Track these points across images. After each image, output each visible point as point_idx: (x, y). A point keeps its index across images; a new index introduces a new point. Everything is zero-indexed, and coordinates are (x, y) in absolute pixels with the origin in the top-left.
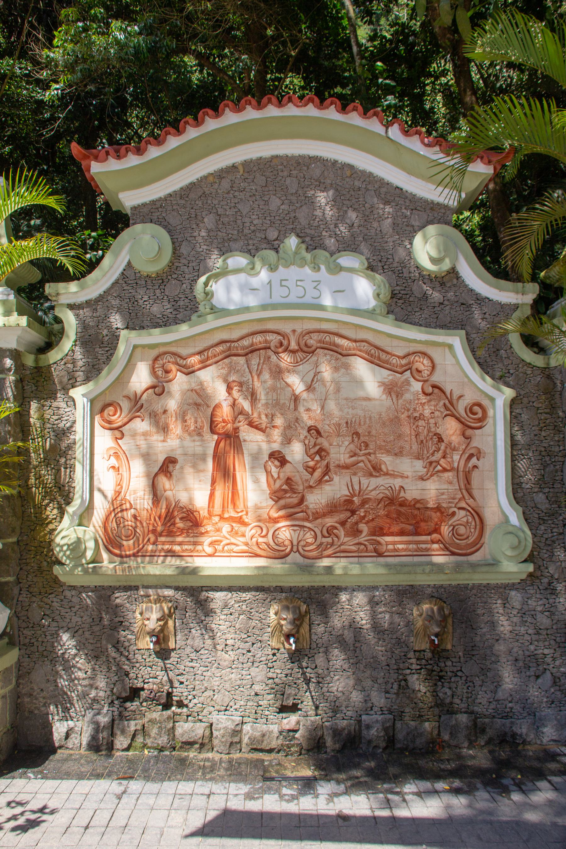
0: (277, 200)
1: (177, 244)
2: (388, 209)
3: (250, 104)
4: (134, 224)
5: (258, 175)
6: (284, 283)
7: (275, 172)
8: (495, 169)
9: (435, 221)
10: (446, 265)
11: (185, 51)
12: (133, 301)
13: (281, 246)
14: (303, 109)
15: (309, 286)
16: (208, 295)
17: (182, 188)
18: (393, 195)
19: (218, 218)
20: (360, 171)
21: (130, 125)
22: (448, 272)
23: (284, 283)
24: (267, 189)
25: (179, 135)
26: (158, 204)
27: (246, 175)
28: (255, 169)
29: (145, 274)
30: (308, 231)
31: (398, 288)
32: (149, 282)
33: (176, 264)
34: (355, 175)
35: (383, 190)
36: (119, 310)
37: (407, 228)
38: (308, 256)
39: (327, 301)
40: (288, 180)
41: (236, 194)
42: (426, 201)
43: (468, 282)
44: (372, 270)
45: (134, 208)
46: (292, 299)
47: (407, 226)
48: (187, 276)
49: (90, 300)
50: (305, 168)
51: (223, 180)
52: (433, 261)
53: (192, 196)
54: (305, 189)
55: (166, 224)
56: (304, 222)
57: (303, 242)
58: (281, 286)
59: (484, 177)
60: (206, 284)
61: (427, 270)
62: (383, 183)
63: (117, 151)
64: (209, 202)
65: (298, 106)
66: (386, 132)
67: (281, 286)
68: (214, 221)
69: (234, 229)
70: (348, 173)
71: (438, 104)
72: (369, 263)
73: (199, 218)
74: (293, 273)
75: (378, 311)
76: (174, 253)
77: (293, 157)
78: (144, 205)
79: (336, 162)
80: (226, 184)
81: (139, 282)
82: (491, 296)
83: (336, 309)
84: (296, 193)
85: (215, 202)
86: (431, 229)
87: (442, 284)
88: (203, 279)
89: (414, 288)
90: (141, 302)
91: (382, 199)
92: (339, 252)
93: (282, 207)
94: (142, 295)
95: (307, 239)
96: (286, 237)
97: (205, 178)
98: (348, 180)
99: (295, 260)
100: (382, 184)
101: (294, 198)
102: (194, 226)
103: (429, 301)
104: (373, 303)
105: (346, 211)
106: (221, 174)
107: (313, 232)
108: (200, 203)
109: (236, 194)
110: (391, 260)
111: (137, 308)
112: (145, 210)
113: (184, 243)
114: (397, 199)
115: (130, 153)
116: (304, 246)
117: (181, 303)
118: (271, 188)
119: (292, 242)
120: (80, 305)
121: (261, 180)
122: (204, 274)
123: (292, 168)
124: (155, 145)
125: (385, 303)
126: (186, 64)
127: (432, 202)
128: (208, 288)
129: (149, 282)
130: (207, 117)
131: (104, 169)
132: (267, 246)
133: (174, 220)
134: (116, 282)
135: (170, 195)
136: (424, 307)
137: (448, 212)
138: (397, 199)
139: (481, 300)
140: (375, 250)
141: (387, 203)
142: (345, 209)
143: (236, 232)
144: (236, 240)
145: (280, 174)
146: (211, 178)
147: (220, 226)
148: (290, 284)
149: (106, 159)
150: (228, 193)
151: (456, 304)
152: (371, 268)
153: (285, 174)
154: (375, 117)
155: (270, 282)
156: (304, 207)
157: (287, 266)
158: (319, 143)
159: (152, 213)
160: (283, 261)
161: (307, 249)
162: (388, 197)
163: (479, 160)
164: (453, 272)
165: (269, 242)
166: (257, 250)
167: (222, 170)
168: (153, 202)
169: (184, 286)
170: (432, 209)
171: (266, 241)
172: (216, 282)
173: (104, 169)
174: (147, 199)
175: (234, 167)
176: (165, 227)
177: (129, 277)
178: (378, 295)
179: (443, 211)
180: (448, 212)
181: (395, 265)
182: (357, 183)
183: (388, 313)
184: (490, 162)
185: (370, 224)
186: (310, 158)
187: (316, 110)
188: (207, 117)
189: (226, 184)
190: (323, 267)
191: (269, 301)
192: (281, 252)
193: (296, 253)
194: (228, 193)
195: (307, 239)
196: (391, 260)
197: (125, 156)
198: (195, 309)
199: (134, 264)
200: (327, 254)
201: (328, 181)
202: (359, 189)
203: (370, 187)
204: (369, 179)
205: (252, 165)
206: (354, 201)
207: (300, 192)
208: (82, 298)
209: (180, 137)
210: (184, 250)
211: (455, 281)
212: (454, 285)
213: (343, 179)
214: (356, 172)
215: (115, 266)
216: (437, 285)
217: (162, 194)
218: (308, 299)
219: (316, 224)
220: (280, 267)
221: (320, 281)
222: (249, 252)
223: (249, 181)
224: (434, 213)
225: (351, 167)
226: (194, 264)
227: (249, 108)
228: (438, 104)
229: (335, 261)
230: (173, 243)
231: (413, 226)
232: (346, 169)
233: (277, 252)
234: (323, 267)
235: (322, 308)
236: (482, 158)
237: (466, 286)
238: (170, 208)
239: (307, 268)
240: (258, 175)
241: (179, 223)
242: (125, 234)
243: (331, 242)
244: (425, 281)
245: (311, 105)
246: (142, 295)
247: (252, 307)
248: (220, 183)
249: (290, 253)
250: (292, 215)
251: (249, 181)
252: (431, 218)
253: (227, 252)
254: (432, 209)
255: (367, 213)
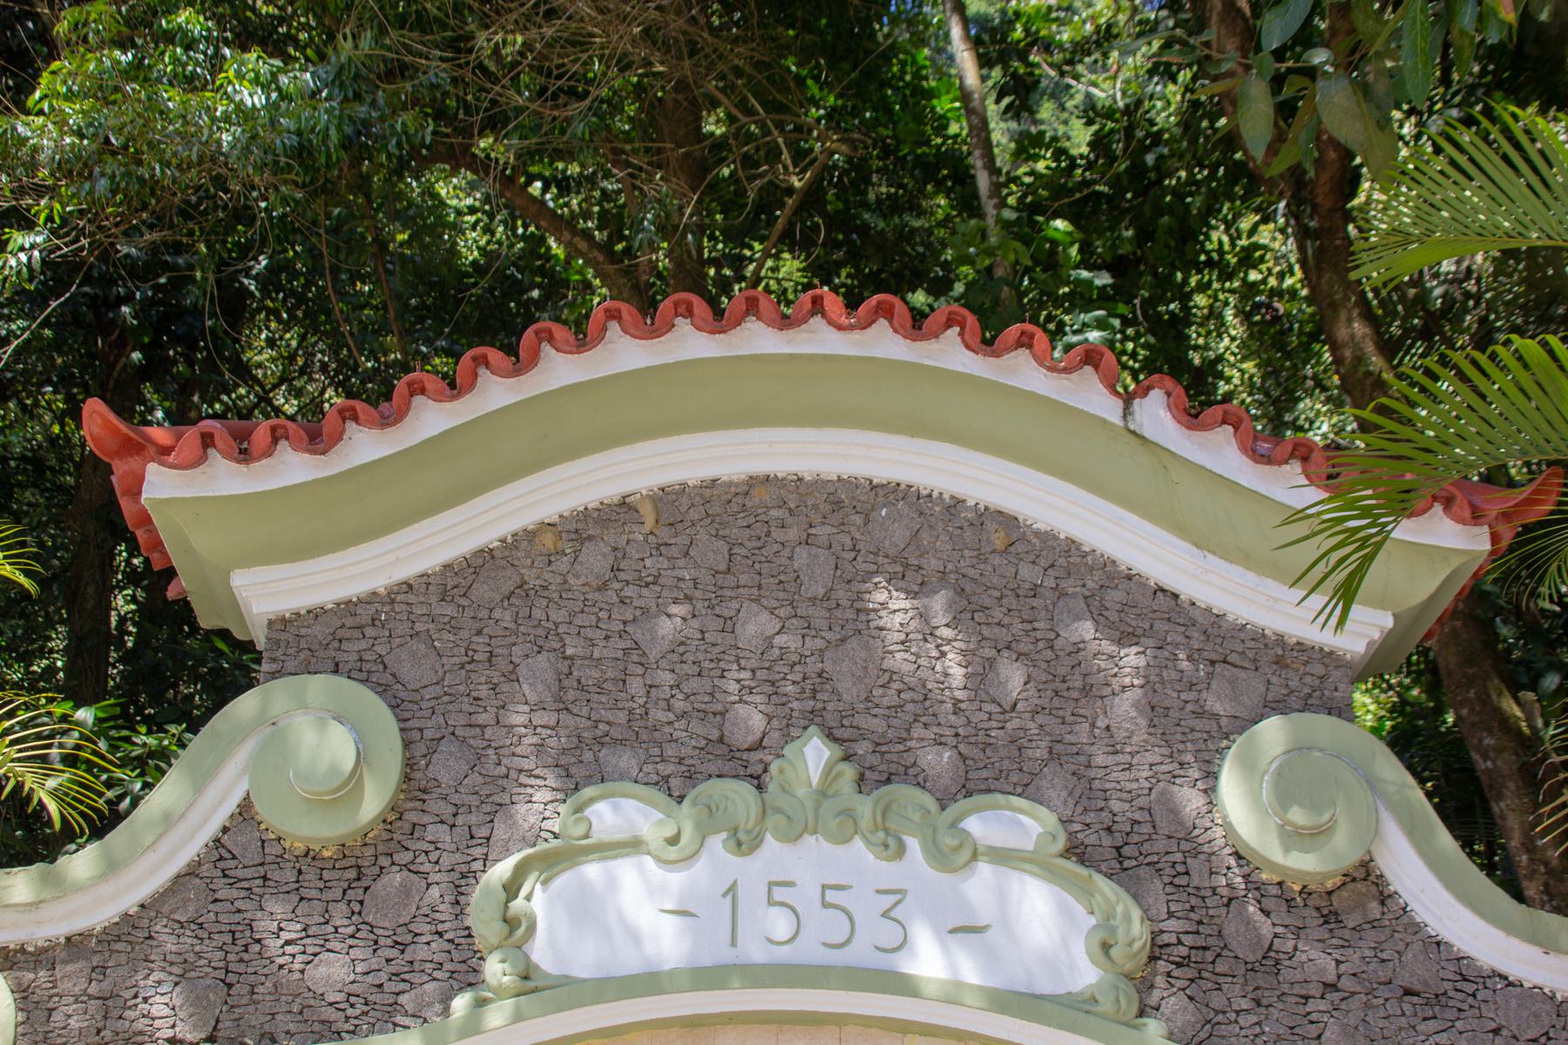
0: (765, 616)
1: (420, 749)
2: (1132, 658)
3: (689, 313)
4: (274, 675)
5: (703, 536)
6: (831, 896)
7: (760, 529)
8: (1495, 538)
9: (1293, 701)
10: (1340, 853)
11: (458, 157)
12: (243, 938)
13: (774, 768)
14: (856, 335)
15: (867, 907)
16: (516, 928)
17: (447, 567)
18: (1147, 612)
19: (563, 666)
20: (1037, 533)
21: (244, 372)
22: (1349, 878)
23: (779, 894)
24: (730, 580)
25: (453, 398)
26: (365, 614)
27: (664, 534)
28: (694, 515)
29: (300, 847)
30: (860, 721)
31: (1172, 924)
32: (310, 875)
33: (412, 817)
34: (1019, 547)
35: (1114, 597)
36: (184, 972)
37: (1200, 724)
38: (865, 807)
39: (928, 960)
40: (802, 556)
41: (629, 591)
42: (1259, 636)
43: (1421, 913)
44: (1082, 860)
45: (280, 624)
46: (809, 951)
47: (1199, 714)
48: (446, 860)
49: (85, 935)
50: (859, 520)
51: (588, 548)
52: (1294, 837)
53: (482, 591)
54: (856, 586)
55: (386, 678)
56: (850, 691)
57: (847, 758)
58: (825, 905)
59: (1456, 562)
60: (511, 888)
61: (1274, 867)
62: (1111, 575)
63: (241, 437)
64: (538, 614)
65: (840, 328)
66: (1127, 412)
67: (825, 905)
68: (550, 676)
69: (616, 707)
70: (999, 540)
71: (1227, 344)
72: (1071, 835)
73: (502, 664)
74: (808, 861)
75: (1106, 1006)
76: (407, 778)
77: (819, 483)
78: (316, 614)
79: (958, 502)
80: (595, 560)
81: (275, 875)
82: (1514, 971)
83: (953, 993)
84: (827, 597)
85: (558, 615)
86: (1272, 733)
87: (1330, 918)
88: (502, 869)
89: (1230, 929)
90: (274, 945)
91: (1112, 626)
92: (969, 794)
93: (779, 640)
94: (277, 924)
95: (862, 748)
96: (788, 738)
97: (530, 535)
98: (997, 560)
99: (819, 818)
100: (1111, 577)
101: (819, 615)
102: (484, 691)
103: (1286, 975)
104: (1086, 975)
105: (991, 662)
106: (580, 528)
107: (878, 725)
108: (507, 617)
109: (629, 591)
110: (1146, 829)
111: (256, 965)
112: (319, 631)
113: (443, 746)
114: (1158, 625)
115: (283, 445)
116: (849, 772)
117: (421, 952)
118: (744, 579)
119: (815, 754)
120: (42, 951)
121: (711, 552)
122: (507, 852)
123: (817, 519)
124: (371, 424)
125: (1129, 977)
126: (442, 204)
127: (1281, 640)
128: (518, 904)
129: (310, 875)
130: (546, 348)
131: (186, 493)
132: (727, 767)
133: (414, 668)
134: (192, 871)
135: (408, 586)
136: (1268, 997)
137: (1336, 675)
138: (1160, 626)
139: (1471, 983)
140: (1086, 795)
141: (1126, 637)
142: (989, 652)
143: (622, 717)
144: (622, 742)
145: (777, 534)
146: (548, 539)
147: (571, 694)
148: (806, 895)
149: (201, 460)
150: (603, 587)
151: (1384, 992)
152: (1077, 851)
153: (793, 534)
154: (1088, 369)
155: (732, 890)
156: (853, 643)
157: (791, 836)
158: (903, 441)
159: (338, 642)
160: (780, 818)
161: (861, 780)
162: (1131, 619)
163: (1438, 508)
164: (1365, 877)
165: (732, 754)
166: (691, 777)
167: (585, 515)
168: (348, 607)
169: (435, 892)
170: (1278, 661)
171: (723, 750)
172: (545, 883)
173: (186, 493)
174: (327, 596)
175: (625, 505)
176: (382, 690)
177: (243, 860)
178: (1106, 947)
179: (1318, 669)
180: (1336, 675)
181: (1161, 845)
182: (1027, 572)
183: (1141, 1014)
184: (1476, 517)
185: (1045, 703)
186: (874, 488)
187: (899, 339)
188: (546, 348)
189: (595, 560)
190: (913, 844)
191: (728, 956)
192: (772, 787)
193: (823, 793)
194: (603, 587)
195: (862, 748)
196: (1146, 829)
197: (268, 453)
198: (467, 975)
199: (262, 809)
200: (930, 802)
201: (933, 564)
202: (1035, 591)
203: (1069, 585)
204: (1066, 559)
205: (685, 501)
206: (1018, 627)
207: (841, 594)
208: (53, 926)
209: (456, 404)
210: (446, 768)
211: (1374, 909)
212: (1373, 924)
213: (981, 558)
214: (1023, 538)
215: (194, 816)
216: (1313, 920)
217: (379, 582)
218: (860, 954)
219: (890, 698)
220: (769, 837)
221: (901, 892)
222: (663, 783)
223: (674, 551)
224: (1296, 679)
225: (1008, 520)
226: (473, 819)
227: (683, 325)
228: (1227, 344)
229: (954, 825)
230: (407, 744)
231: (1216, 716)
232: (990, 526)
233: (760, 787)
234: (913, 844)
235: (905, 986)
236: (1448, 503)
237: (1417, 928)
238: (402, 628)
239: (858, 843)
240: (703, 536)
241: (430, 677)
242: (245, 705)
243: (938, 761)
244: (1269, 903)
245: (882, 323)
246: (277, 924)
247: (673, 973)
248: (577, 553)
249: (801, 792)
250: (813, 666)
251: (674, 551)
252: (1277, 692)
253: (589, 780)
254: (1278, 661)
255: (1062, 671)
